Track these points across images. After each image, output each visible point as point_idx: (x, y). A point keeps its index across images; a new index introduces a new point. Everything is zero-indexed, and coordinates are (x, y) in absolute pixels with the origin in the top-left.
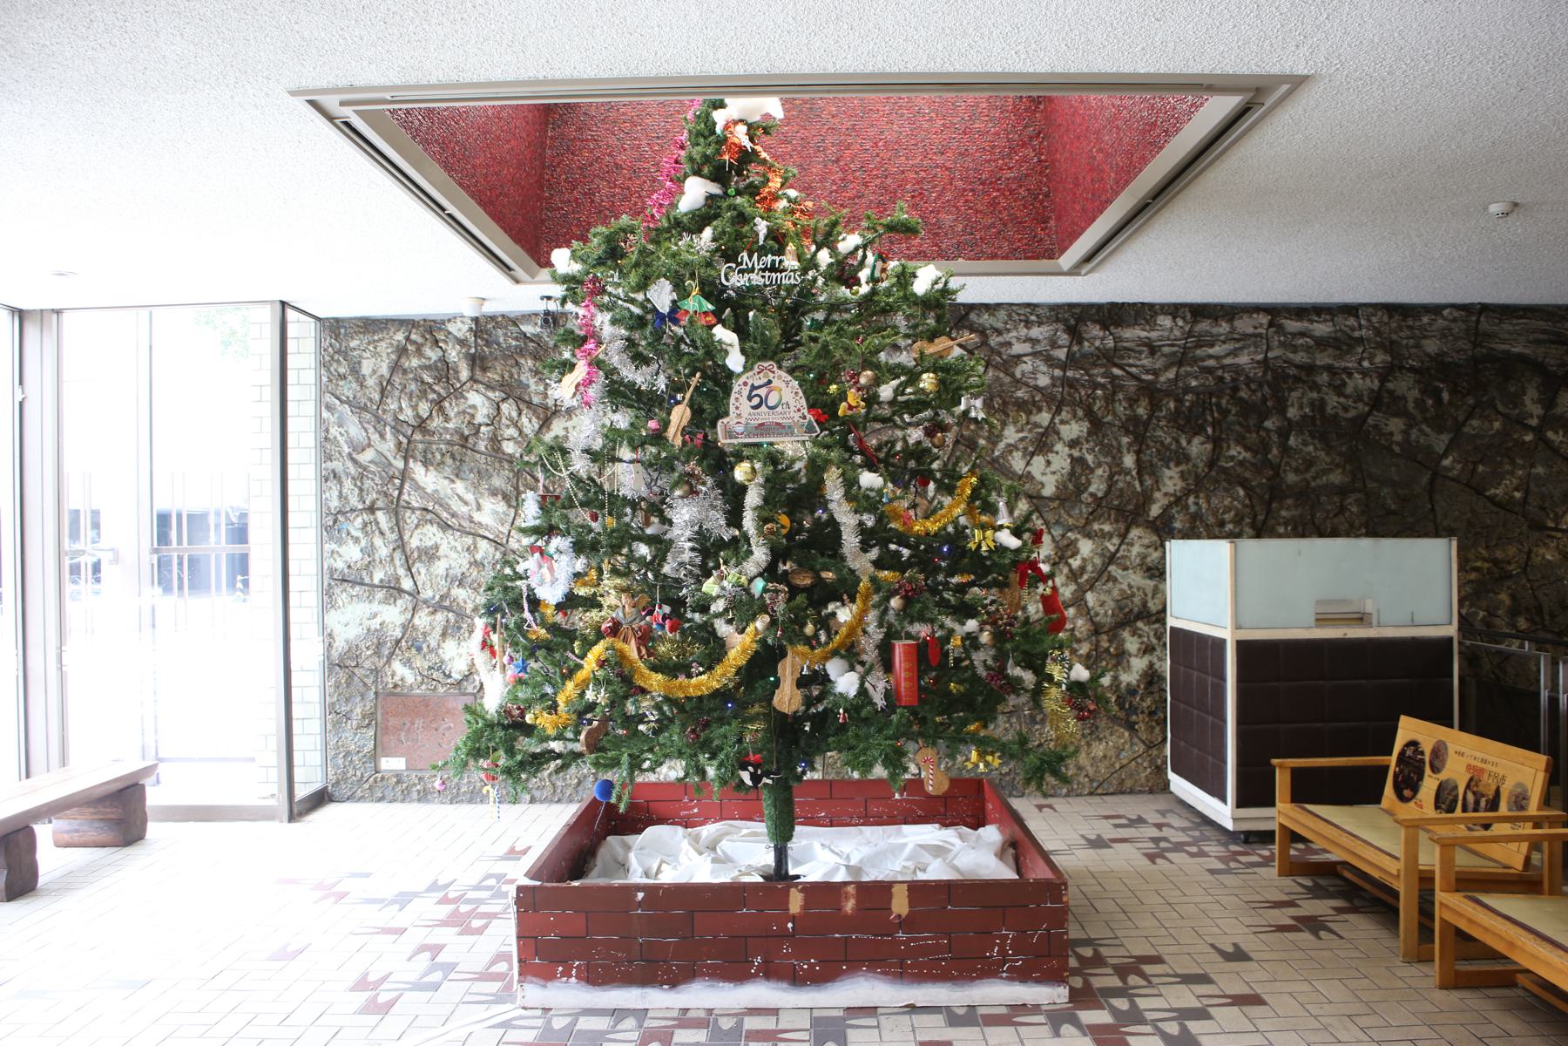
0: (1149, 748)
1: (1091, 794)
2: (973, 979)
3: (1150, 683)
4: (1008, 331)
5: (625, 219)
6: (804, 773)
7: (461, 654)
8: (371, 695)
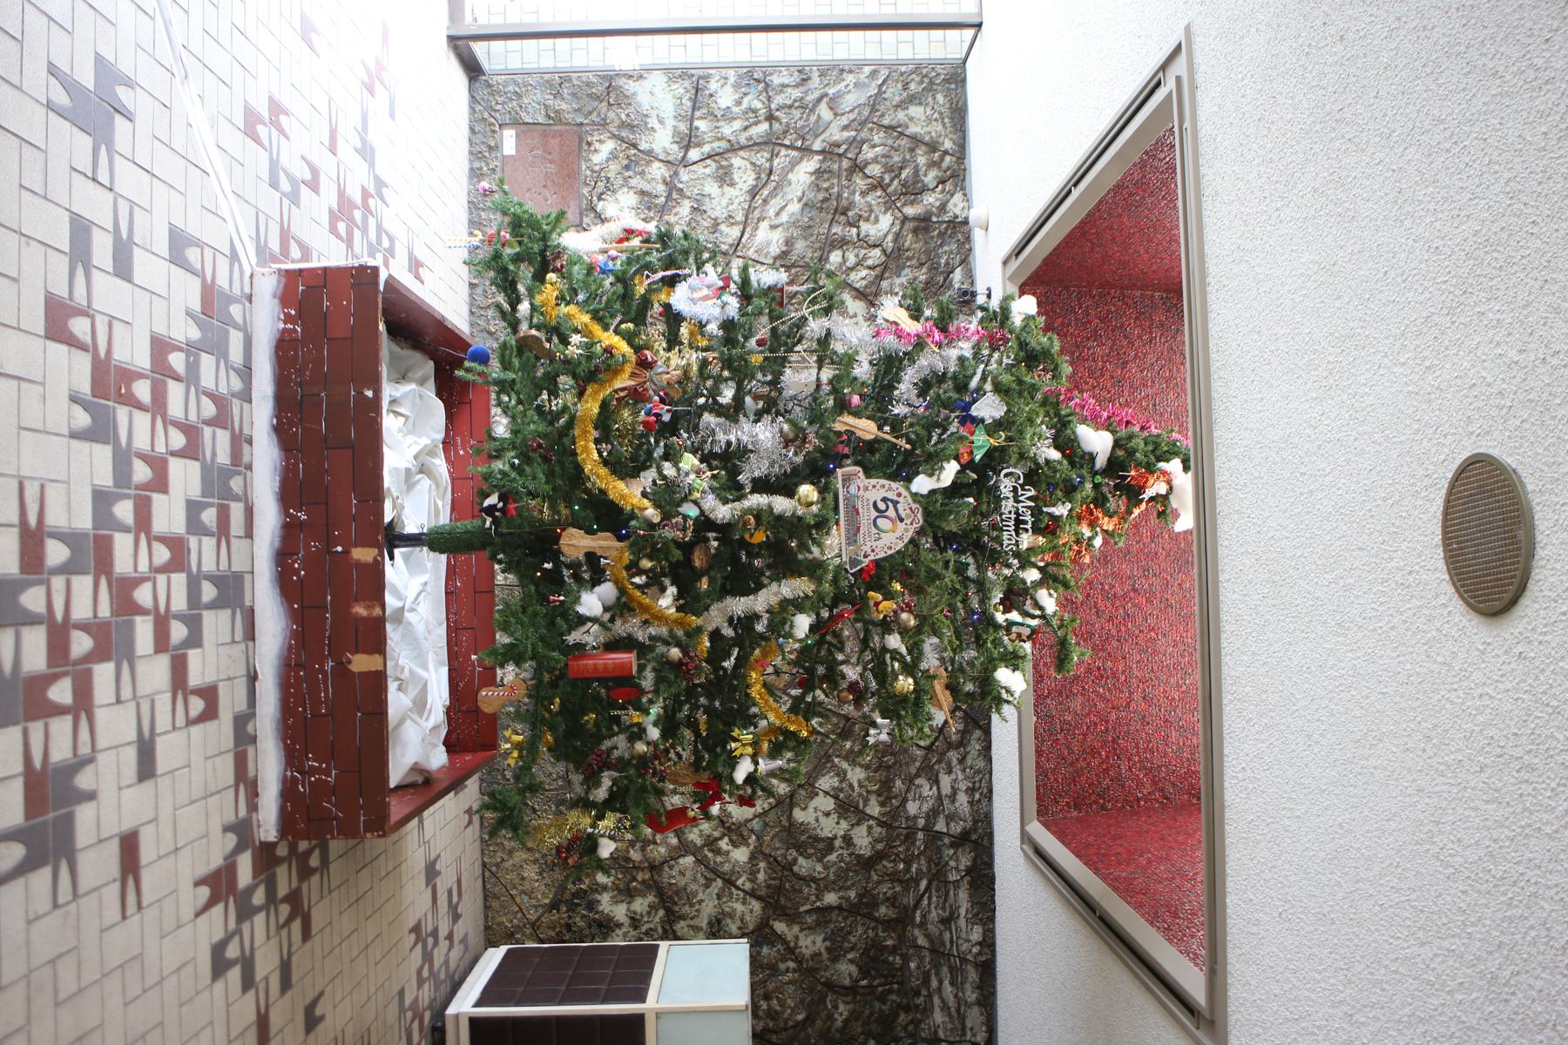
0: (533, 925)
1: (484, 865)
2: (284, 740)
3: (600, 925)
4: (964, 771)
5: (1067, 369)
6: (500, 562)
7: (622, 211)
8: (580, 119)
